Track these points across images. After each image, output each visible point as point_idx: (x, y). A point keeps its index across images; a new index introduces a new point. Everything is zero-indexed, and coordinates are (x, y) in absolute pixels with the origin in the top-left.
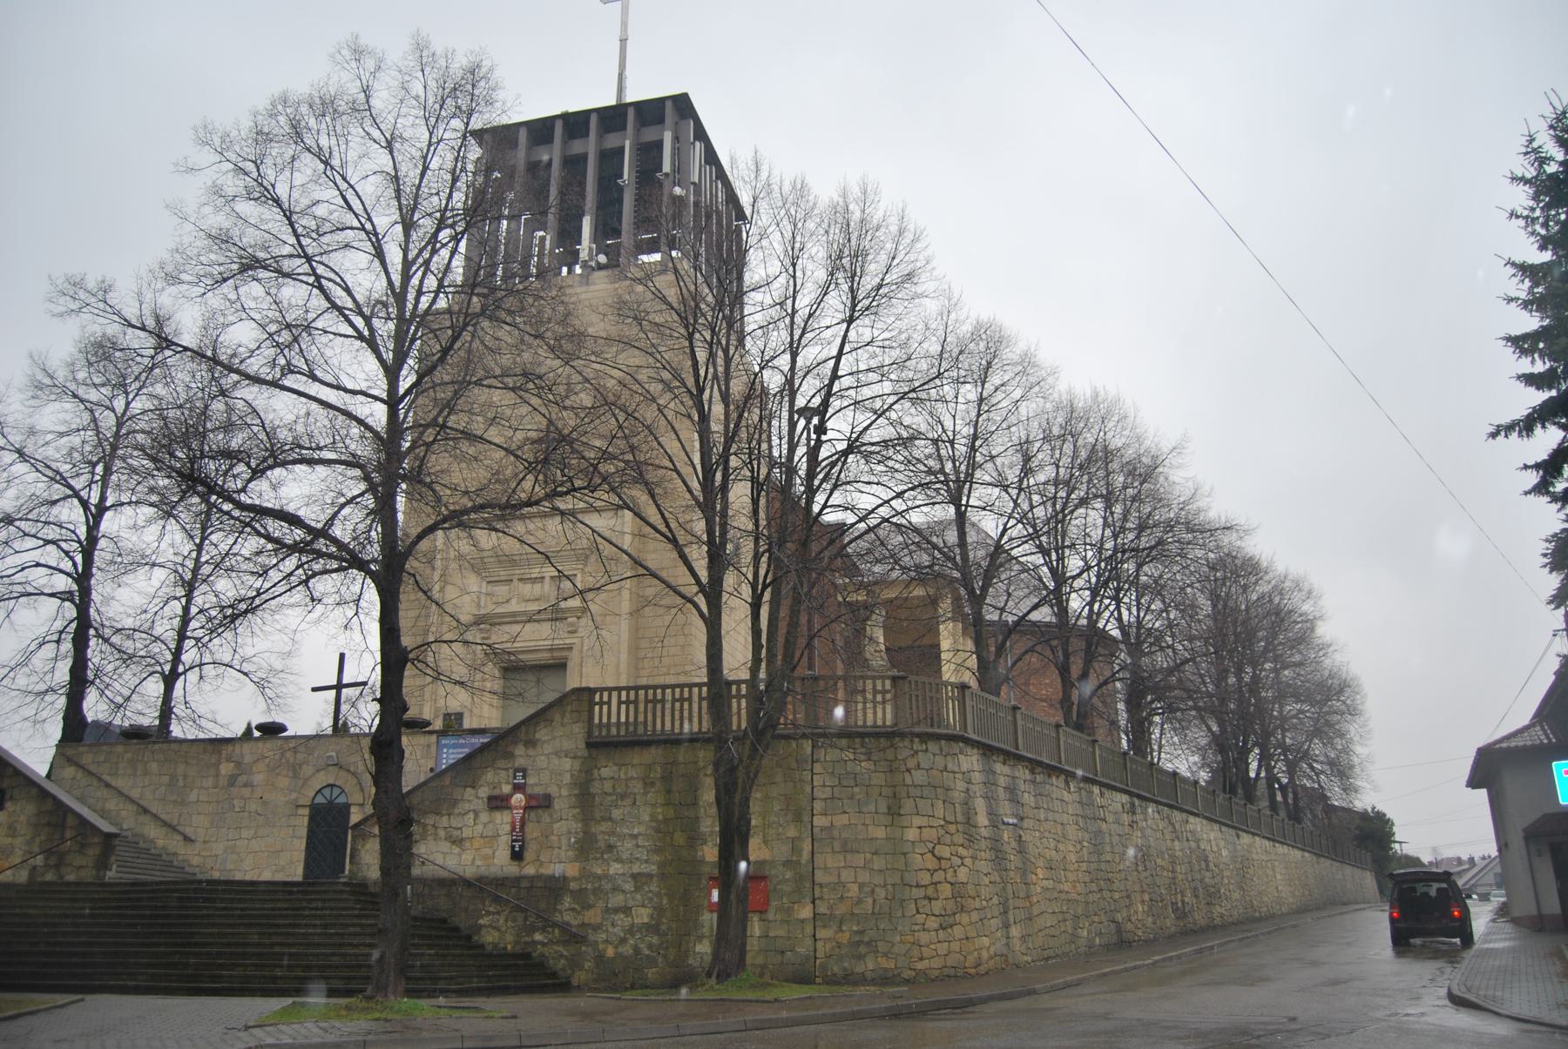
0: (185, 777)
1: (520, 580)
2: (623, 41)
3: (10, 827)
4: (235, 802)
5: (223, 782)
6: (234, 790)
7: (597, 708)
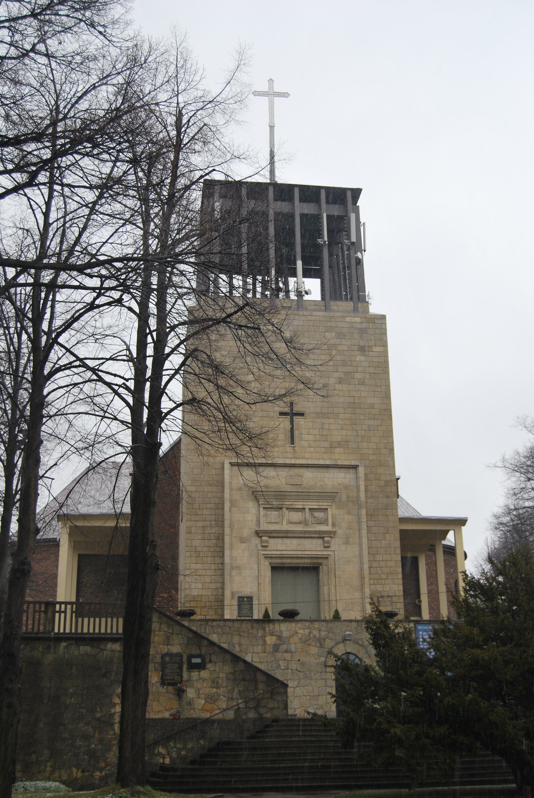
0: (240, 645)
1: (287, 508)
2: (272, 127)
3: (213, 682)
4: (281, 663)
5: (269, 649)
6: (279, 655)
7: (57, 615)
